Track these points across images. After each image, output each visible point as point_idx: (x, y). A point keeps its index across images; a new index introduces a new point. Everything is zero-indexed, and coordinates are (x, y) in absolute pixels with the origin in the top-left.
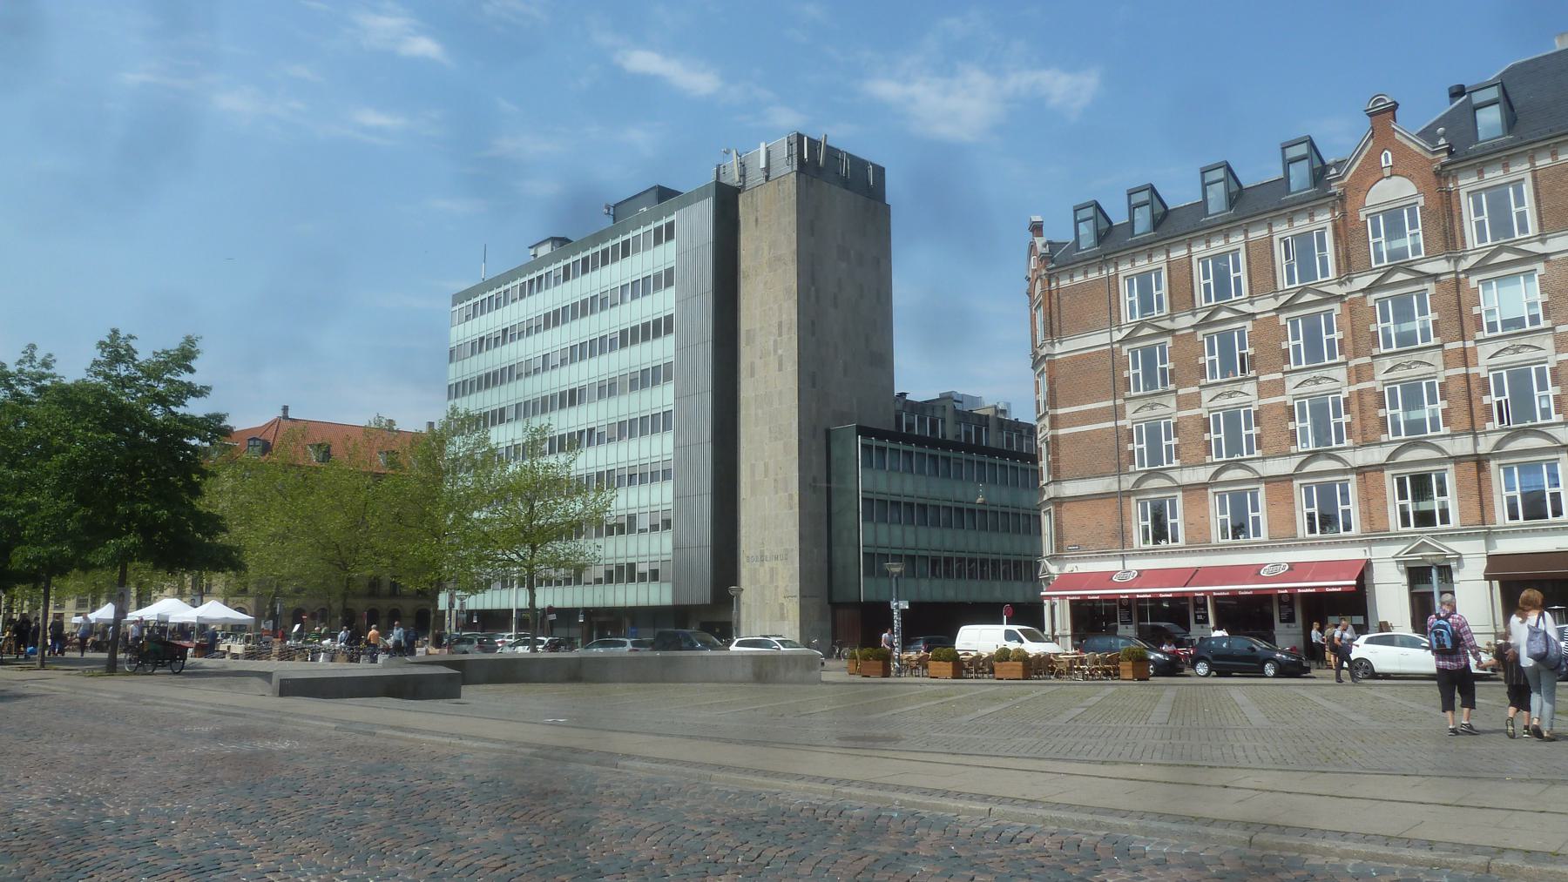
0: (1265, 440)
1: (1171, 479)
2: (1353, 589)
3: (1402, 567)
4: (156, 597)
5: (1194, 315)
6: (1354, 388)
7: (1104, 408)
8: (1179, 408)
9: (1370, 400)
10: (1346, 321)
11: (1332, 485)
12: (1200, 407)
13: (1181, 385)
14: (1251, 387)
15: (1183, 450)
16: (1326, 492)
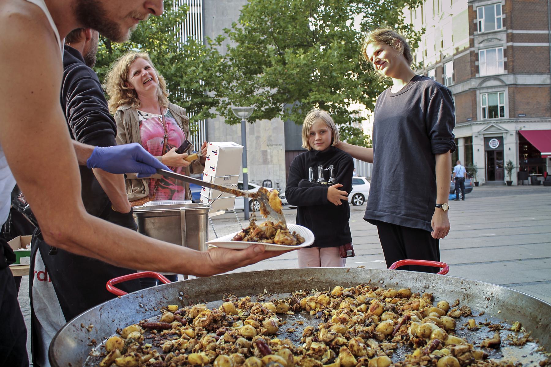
7: (542, 34)
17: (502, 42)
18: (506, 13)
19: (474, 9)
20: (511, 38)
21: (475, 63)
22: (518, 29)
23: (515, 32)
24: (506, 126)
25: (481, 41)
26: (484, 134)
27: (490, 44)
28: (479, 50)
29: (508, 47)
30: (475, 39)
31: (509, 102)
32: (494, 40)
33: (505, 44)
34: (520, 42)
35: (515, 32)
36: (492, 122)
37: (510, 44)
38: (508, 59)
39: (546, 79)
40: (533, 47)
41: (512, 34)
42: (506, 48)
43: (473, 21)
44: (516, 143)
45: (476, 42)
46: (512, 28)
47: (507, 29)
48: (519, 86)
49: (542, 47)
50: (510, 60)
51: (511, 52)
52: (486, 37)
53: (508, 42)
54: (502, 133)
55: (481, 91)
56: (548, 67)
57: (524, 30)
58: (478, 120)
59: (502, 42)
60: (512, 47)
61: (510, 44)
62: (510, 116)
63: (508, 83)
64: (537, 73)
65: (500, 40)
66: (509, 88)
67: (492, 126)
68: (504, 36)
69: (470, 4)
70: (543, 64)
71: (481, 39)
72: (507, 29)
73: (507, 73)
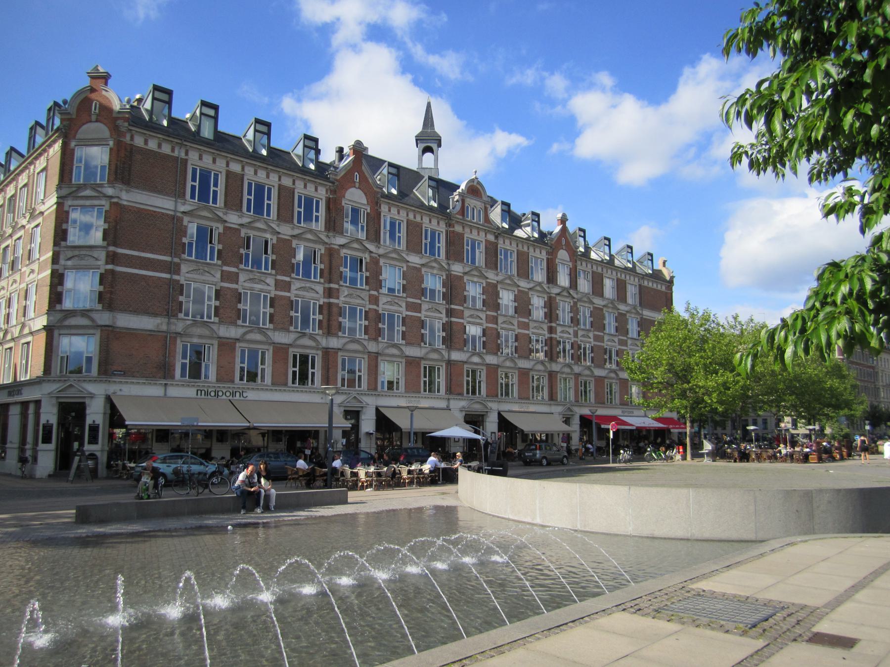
0: (276, 318)
1: (93, 320)
2: (349, 429)
3: (54, 401)
4: (110, 628)
5: (293, 229)
6: (326, 300)
7: (162, 261)
8: (222, 280)
9: (335, 310)
10: (326, 259)
11: (256, 351)
12: (237, 284)
13: (225, 263)
14: (271, 281)
15: (221, 311)
16: (253, 354)
17: (99, 263)
18: (109, 223)
19: (66, 208)
20: (112, 258)
21: (57, 288)
22: (125, 248)
23: (120, 251)
24: (91, 388)
25: (69, 256)
26: (58, 398)
27: (83, 262)
28: (65, 269)
29: (106, 270)
30: (62, 253)
31: (100, 352)
32: (89, 258)
33: (103, 265)
34: (126, 267)
35: (120, 251)
36: (72, 379)
37: (110, 267)
38: (105, 288)
39: (162, 324)
40: (146, 276)
41: (115, 254)
42: (103, 272)
43: (61, 226)
44: (105, 414)
45: (62, 257)
46: (115, 245)
47: (108, 245)
48: (118, 330)
49: (159, 278)
50: (107, 289)
51: (110, 278)
52: (77, 253)
53: (107, 263)
54: (84, 397)
55: (62, 332)
56: (167, 307)
57: (134, 250)
58: (53, 374)
59: (99, 263)
60: (112, 272)
61: (110, 267)
62: (100, 372)
63: (100, 323)
64: (148, 313)
65: (97, 259)
66: (102, 330)
67: (71, 386)
68: (102, 255)
69: (61, 201)
70: (160, 302)
71: (70, 254)
72: (108, 245)
73: (101, 308)
